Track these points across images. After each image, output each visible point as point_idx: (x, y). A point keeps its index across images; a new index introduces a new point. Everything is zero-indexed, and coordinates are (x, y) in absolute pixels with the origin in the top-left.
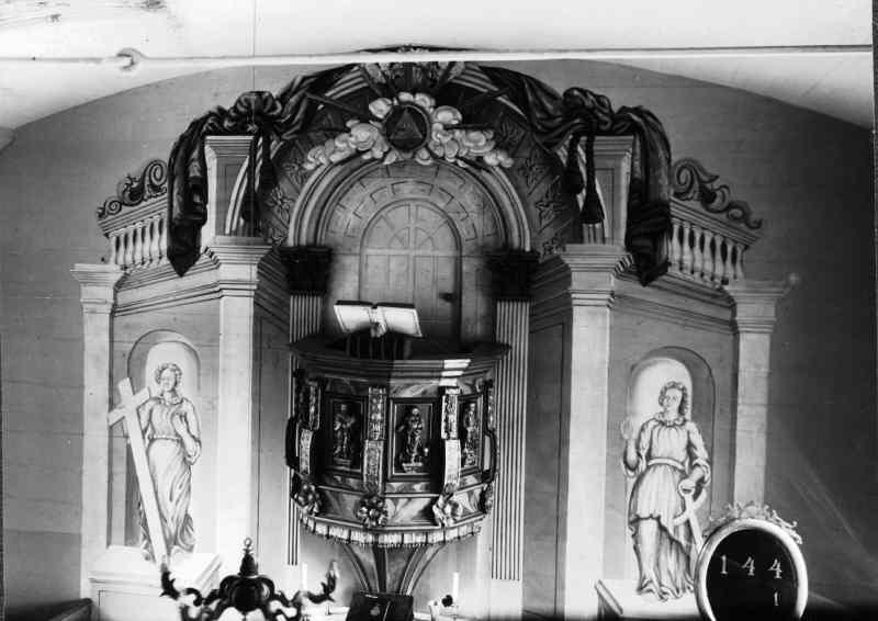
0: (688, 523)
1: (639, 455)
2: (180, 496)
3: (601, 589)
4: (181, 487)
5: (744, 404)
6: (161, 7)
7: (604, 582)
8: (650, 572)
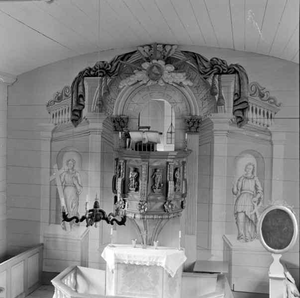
1: (238, 189)
7: (226, 235)
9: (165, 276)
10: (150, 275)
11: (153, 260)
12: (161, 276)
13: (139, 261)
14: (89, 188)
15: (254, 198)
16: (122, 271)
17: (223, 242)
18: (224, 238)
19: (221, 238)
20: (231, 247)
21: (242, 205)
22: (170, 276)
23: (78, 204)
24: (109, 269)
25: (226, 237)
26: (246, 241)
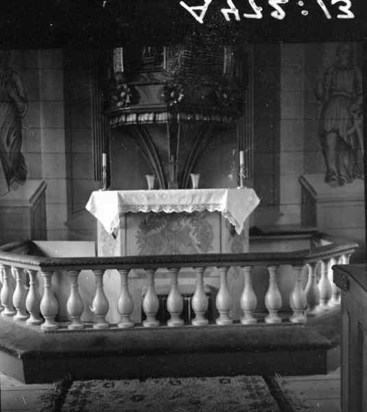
0: (355, 134)
1: (325, 90)
2: (14, 141)
3: (302, 181)
4: (14, 135)
5: (113, 253)
6: (127, 206)
7: (305, 176)
8: (333, 167)
9: (226, 233)
10: (194, 234)
11: (200, 200)
12: (216, 230)
13: (172, 206)
14: (41, 103)
15: (354, 105)
16: (134, 231)
17: (300, 187)
18: (301, 179)
19: (297, 180)
20: (315, 197)
21: (331, 119)
22: (233, 232)
23: (21, 136)
24: (103, 228)
25: (305, 180)
26: (341, 183)
